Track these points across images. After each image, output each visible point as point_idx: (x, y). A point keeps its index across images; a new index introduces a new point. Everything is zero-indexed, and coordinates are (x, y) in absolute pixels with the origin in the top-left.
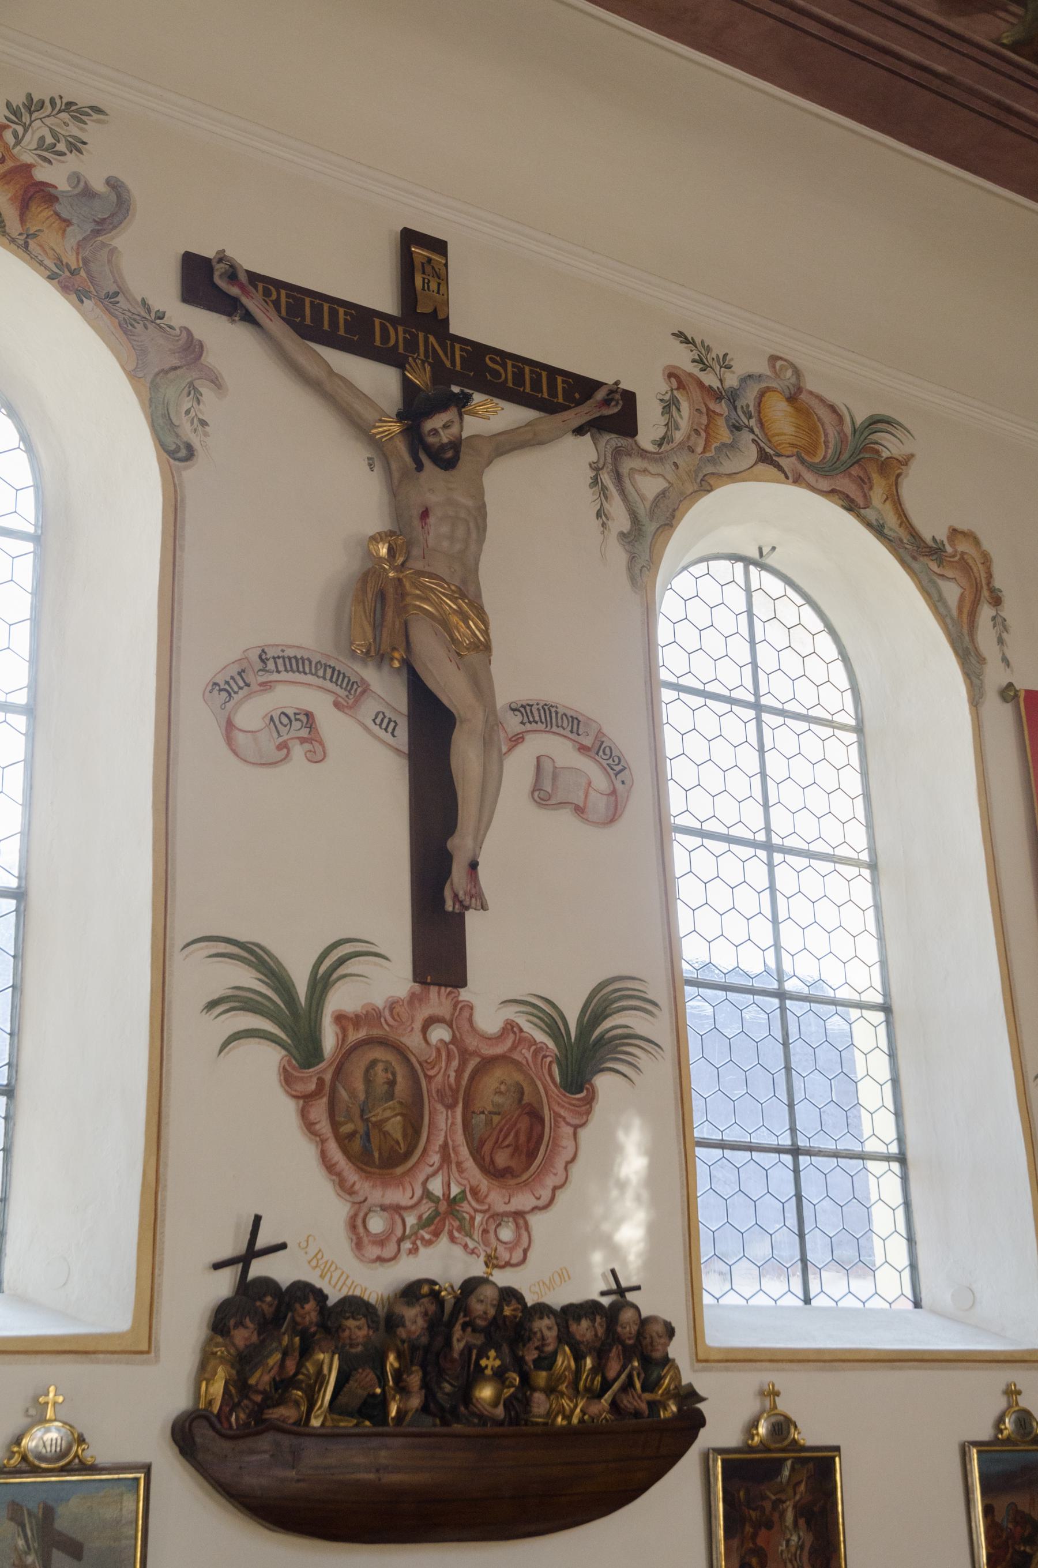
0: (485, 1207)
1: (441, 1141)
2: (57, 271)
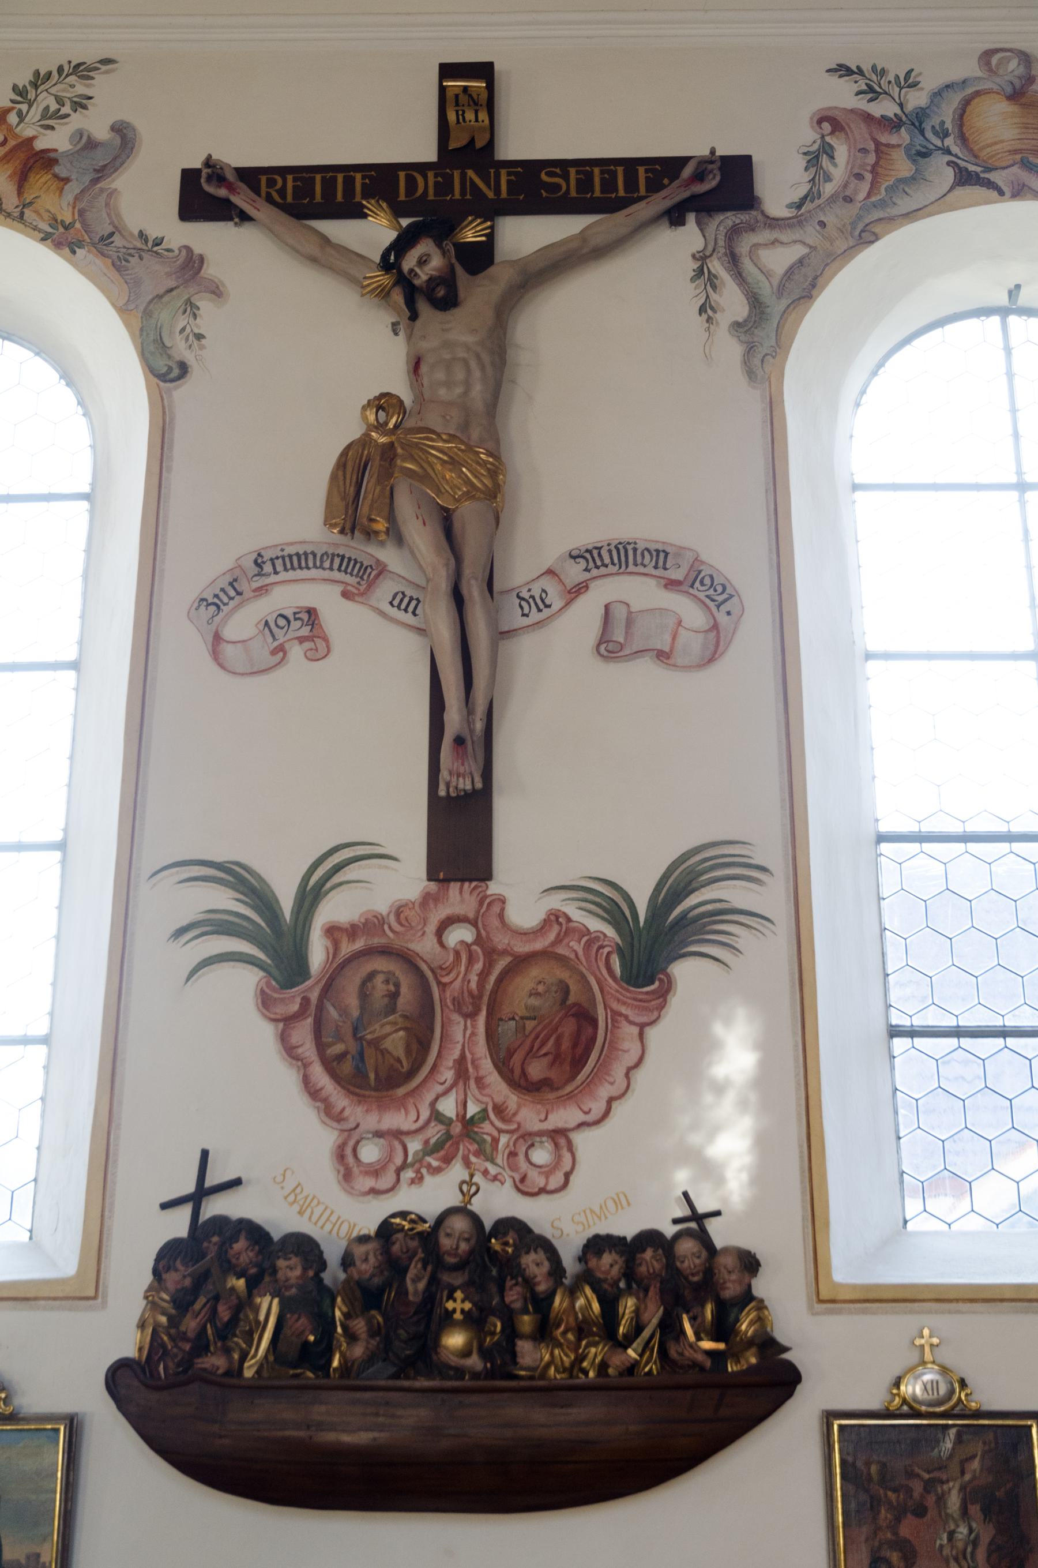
0: (514, 1127)
1: (456, 1054)
2: (50, 230)
